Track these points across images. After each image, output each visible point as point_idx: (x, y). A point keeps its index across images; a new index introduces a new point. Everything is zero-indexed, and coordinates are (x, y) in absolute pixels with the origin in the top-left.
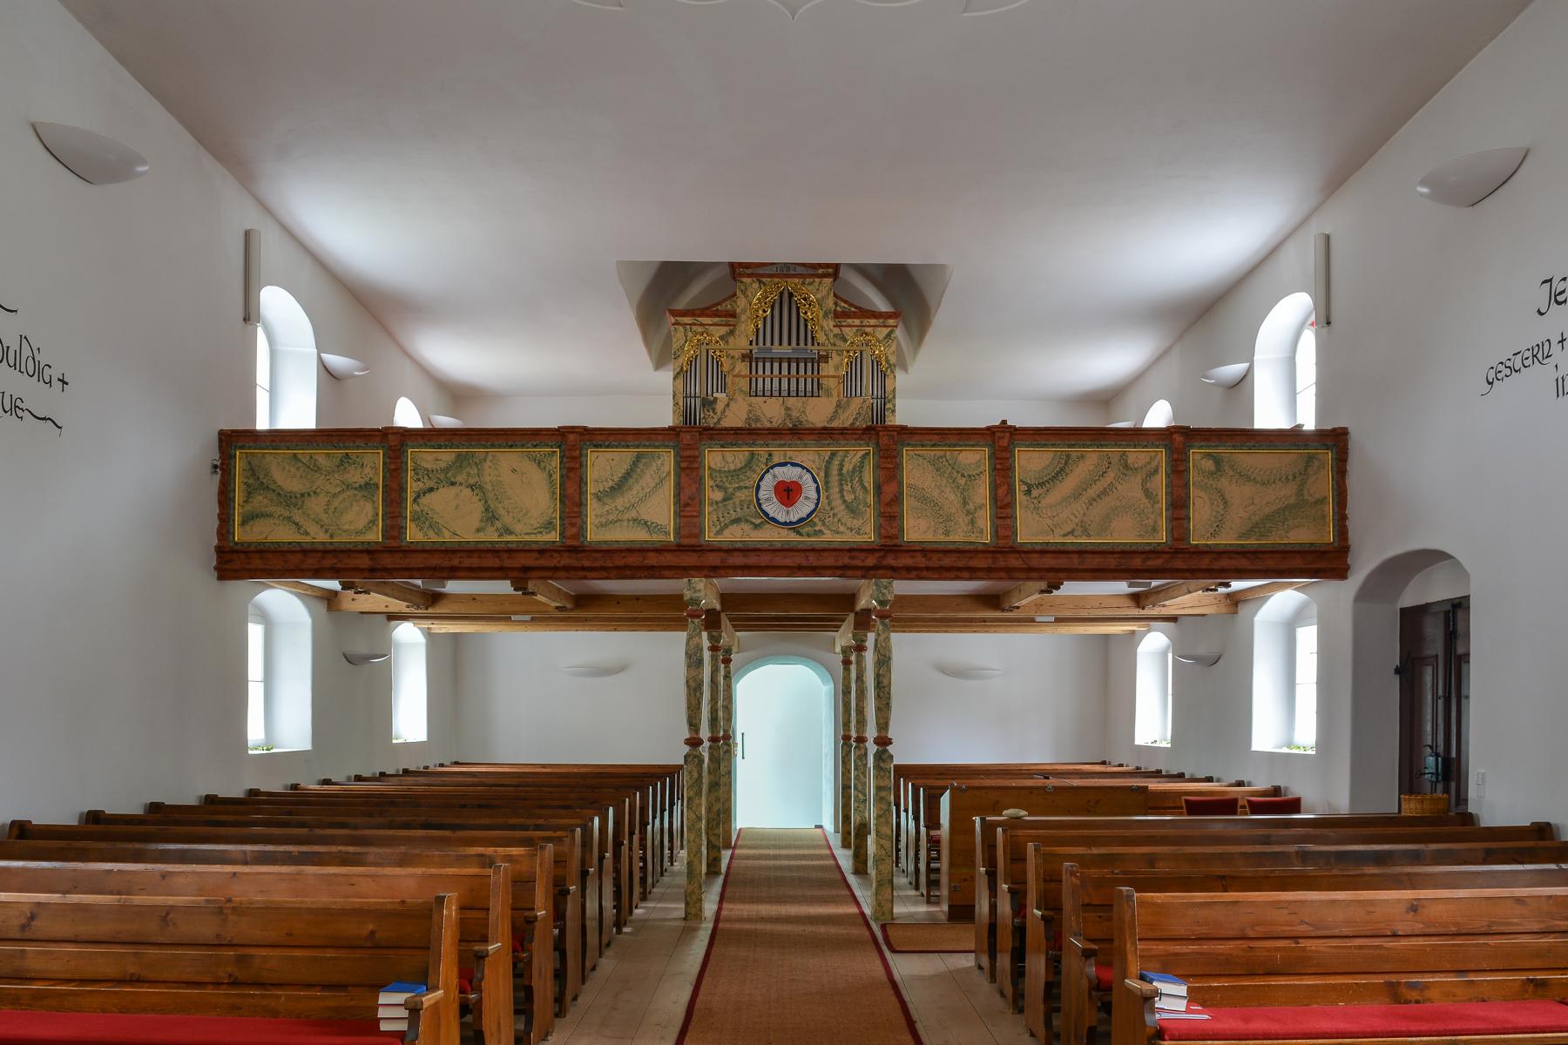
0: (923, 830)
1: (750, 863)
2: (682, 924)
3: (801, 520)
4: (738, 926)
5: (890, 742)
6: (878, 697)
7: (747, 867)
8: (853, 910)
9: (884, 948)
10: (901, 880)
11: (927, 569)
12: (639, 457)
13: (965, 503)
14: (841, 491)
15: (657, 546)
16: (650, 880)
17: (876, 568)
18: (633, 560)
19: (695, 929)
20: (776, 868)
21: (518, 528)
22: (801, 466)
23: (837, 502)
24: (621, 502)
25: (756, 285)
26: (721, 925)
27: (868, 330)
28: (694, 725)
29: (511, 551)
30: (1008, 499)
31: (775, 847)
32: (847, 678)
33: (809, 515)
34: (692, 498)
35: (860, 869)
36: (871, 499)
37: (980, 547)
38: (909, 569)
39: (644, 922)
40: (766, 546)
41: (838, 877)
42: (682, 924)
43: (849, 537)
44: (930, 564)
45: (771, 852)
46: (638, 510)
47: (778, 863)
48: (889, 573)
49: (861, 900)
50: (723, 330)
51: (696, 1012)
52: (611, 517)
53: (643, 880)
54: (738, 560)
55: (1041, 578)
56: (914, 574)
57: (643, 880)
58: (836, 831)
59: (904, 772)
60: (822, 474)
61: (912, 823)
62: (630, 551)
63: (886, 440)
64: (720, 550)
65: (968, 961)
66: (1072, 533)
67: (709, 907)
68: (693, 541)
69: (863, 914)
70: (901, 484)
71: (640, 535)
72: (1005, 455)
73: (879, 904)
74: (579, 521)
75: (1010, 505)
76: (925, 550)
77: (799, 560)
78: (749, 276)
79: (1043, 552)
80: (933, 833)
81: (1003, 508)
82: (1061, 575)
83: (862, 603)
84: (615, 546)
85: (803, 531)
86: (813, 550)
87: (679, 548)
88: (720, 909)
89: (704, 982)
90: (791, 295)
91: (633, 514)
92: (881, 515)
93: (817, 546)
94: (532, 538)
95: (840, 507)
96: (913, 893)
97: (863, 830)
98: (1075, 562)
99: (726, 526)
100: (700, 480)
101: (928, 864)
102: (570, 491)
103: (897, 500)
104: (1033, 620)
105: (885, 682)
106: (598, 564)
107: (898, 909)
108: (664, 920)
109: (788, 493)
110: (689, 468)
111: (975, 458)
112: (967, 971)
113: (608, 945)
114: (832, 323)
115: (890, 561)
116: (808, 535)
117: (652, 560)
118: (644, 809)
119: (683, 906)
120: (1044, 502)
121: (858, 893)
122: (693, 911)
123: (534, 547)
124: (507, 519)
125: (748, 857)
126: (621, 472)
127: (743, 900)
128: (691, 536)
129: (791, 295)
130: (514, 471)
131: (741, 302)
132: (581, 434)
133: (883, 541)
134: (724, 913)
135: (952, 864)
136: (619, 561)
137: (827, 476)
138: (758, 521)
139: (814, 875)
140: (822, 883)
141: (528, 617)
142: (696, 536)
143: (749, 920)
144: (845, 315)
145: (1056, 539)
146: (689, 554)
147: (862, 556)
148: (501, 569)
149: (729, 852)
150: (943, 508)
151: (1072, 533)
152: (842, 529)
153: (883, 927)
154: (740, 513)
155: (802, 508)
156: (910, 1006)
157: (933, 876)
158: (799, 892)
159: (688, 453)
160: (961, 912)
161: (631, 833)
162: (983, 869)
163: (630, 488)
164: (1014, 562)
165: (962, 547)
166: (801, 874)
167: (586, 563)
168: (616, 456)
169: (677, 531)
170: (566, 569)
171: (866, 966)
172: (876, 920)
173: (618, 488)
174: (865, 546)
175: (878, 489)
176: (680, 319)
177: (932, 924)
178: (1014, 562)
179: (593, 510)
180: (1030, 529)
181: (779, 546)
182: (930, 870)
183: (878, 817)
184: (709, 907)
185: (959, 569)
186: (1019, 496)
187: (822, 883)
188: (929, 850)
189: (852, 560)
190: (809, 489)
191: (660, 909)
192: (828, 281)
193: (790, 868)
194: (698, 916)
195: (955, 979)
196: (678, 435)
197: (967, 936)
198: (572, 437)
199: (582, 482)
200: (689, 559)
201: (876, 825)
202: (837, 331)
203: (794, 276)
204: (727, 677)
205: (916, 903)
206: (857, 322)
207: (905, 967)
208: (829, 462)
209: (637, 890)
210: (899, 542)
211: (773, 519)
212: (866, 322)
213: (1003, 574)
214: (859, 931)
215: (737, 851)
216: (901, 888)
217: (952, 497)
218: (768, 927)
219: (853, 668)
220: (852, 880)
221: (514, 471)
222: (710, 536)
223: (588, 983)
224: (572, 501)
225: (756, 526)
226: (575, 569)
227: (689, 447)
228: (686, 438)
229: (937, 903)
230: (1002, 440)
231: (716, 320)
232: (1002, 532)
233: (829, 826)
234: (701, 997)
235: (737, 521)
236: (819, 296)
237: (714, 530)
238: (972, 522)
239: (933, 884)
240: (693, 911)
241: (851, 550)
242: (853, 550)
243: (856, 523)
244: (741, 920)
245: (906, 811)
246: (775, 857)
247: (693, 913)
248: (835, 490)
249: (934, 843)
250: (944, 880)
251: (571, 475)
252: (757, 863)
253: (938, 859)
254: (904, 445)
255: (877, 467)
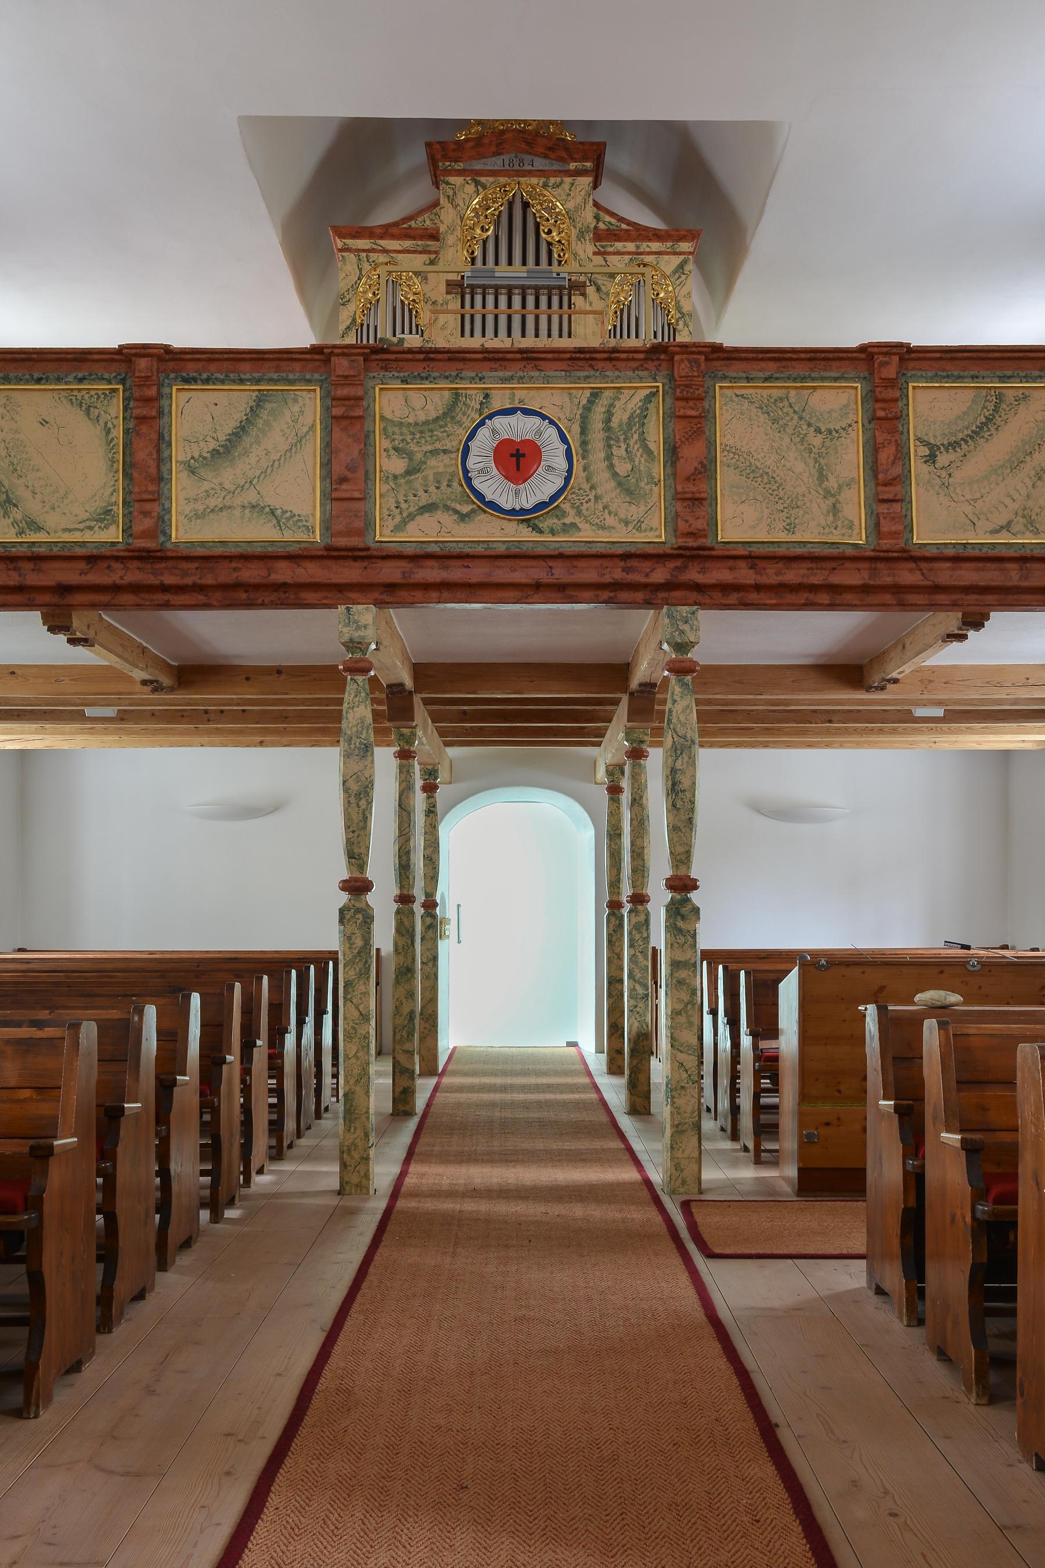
0: (746, 1041)
1: (463, 1097)
2: (333, 1201)
3: (541, 506)
4: (429, 1205)
5: (693, 885)
6: (673, 807)
7: (459, 1105)
8: (630, 1175)
9: (691, 1247)
10: (708, 1125)
11: (758, 588)
12: (261, 401)
13: (822, 477)
14: (609, 457)
15: (292, 549)
16: (290, 1125)
17: (669, 586)
18: (252, 574)
19: (352, 1212)
20: (503, 1106)
21: (51, 520)
22: (542, 413)
23: (602, 476)
24: (229, 475)
25: (470, 188)
26: (400, 1204)
27: (648, 259)
28: (356, 855)
29: (37, 559)
30: (896, 471)
31: (504, 1073)
32: (615, 815)
33: (554, 498)
34: (352, 468)
35: (639, 1104)
36: (659, 470)
37: (849, 552)
38: (726, 588)
39: (271, 1196)
40: (480, 549)
41: (604, 1119)
42: (333, 1201)
43: (620, 535)
44: (764, 580)
45: (499, 1081)
46: (252, 487)
47: (508, 1097)
48: (694, 596)
49: (643, 1157)
50: (418, 261)
51: (317, 1401)
52: (212, 502)
53: (276, 1127)
54: (431, 573)
55: (954, 605)
56: (733, 598)
57: (276, 1127)
58: (599, 1050)
59: (712, 957)
60: (576, 428)
61: (724, 1031)
62: (246, 558)
63: (692, 372)
64: (400, 557)
65: (853, 1277)
66: (1007, 527)
67: (383, 1172)
68: (354, 541)
69: (648, 1183)
70: (711, 444)
71: (261, 532)
72: (891, 394)
73: (677, 1166)
74: (156, 508)
75: (903, 479)
76: (753, 557)
77: (536, 573)
78: (460, 173)
79: (957, 559)
80: (764, 1044)
81: (888, 488)
82: (990, 598)
83: (641, 673)
84: (219, 551)
85: (544, 525)
86: (561, 556)
87: (331, 554)
88: (403, 1174)
89: (349, 1324)
90: (526, 205)
91: (251, 496)
92: (679, 497)
93: (567, 550)
94: (77, 537)
95: (607, 486)
96: (728, 1145)
97: (645, 1044)
98: (1013, 576)
99: (411, 517)
100: (366, 439)
101: (756, 1097)
102: (141, 456)
103: (706, 470)
104: (907, 717)
105: (686, 783)
106: (189, 581)
107: (710, 1174)
108: (304, 1194)
109: (517, 459)
110: (346, 416)
111: (840, 401)
112: (852, 1297)
113: (186, 1244)
114: (590, 248)
115: (693, 574)
116: (553, 532)
117: (284, 573)
118: (278, 1010)
119: (336, 1168)
120: (958, 475)
121: (637, 1146)
122: (355, 1179)
123: (79, 551)
124: (32, 506)
125: (461, 1089)
126: (229, 426)
127: (445, 1158)
128: (350, 533)
129: (526, 205)
130: (44, 422)
131: (447, 216)
132: (160, 359)
133: (681, 542)
134: (409, 1181)
135: (804, 1096)
136: (224, 574)
137: (584, 431)
138: (466, 509)
139: (564, 1116)
140: (580, 1130)
141: (110, 712)
142: (360, 533)
143: (451, 1194)
144: (613, 235)
145: (979, 538)
146: (344, 567)
147: (646, 565)
148: (20, 589)
149: (433, 1081)
150: (787, 480)
151: (1007, 527)
152: (610, 521)
153: (686, 1206)
154: (435, 496)
155: (542, 486)
156: (760, 1383)
157: (764, 1118)
158: (540, 1145)
159: (345, 391)
160: (831, 1178)
161: (247, 1046)
162: (888, 1104)
163: (246, 453)
164: (907, 576)
165: (817, 550)
166: (544, 1114)
167: (169, 580)
168: (221, 398)
169: (327, 525)
170: (135, 588)
171: (658, 1285)
172: (673, 1193)
173: (225, 451)
174: (651, 550)
175: (673, 452)
176: (351, 242)
177: (766, 1201)
178: (907, 576)
179: (182, 491)
180: (937, 520)
181: (502, 549)
182: (758, 1108)
183: (674, 1014)
184: (383, 1172)
185: (813, 588)
186: (916, 466)
187: (580, 1130)
188: (758, 1075)
189: (626, 578)
190: (554, 455)
191: (304, 1175)
192: (586, 181)
193: (526, 1106)
194: (362, 1187)
195: (826, 1315)
196: (327, 361)
197: (846, 1224)
198: (143, 363)
199: (161, 442)
200: (349, 573)
201: (672, 1028)
202: (599, 260)
203: (530, 173)
204: (431, 812)
205: (734, 1163)
206: (631, 246)
207: (741, 1289)
208: (588, 409)
209: (261, 1142)
210: (708, 542)
211: (493, 505)
212: (644, 246)
213: (888, 598)
214: (644, 1215)
215: (446, 1080)
216: (712, 1139)
217: (800, 467)
218: (483, 1207)
219: (625, 798)
220: (626, 1123)
221: (44, 422)
222: (383, 533)
223: (120, 1331)
224: (144, 474)
225: (463, 517)
226: (150, 589)
227: (347, 380)
228: (342, 365)
229: (775, 1163)
230: (885, 370)
231: (408, 244)
232: (886, 527)
233: (588, 1045)
234: (335, 1361)
235: (429, 508)
236: (570, 205)
237: (391, 524)
238: (835, 510)
239: (766, 1127)
240: (355, 1179)
241: (626, 556)
242: (629, 557)
243: (635, 512)
244: (437, 1194)
245: (714, 1012)
246: (504, 1089)
247: (353, 1181)
248: (598, 454)
249: (768, 1065)
250: (788, 1123)
251: (144, 429)
252: (474, 1097)
253: (775, 1090)
254: (715, 378)
255: (672, 416)
